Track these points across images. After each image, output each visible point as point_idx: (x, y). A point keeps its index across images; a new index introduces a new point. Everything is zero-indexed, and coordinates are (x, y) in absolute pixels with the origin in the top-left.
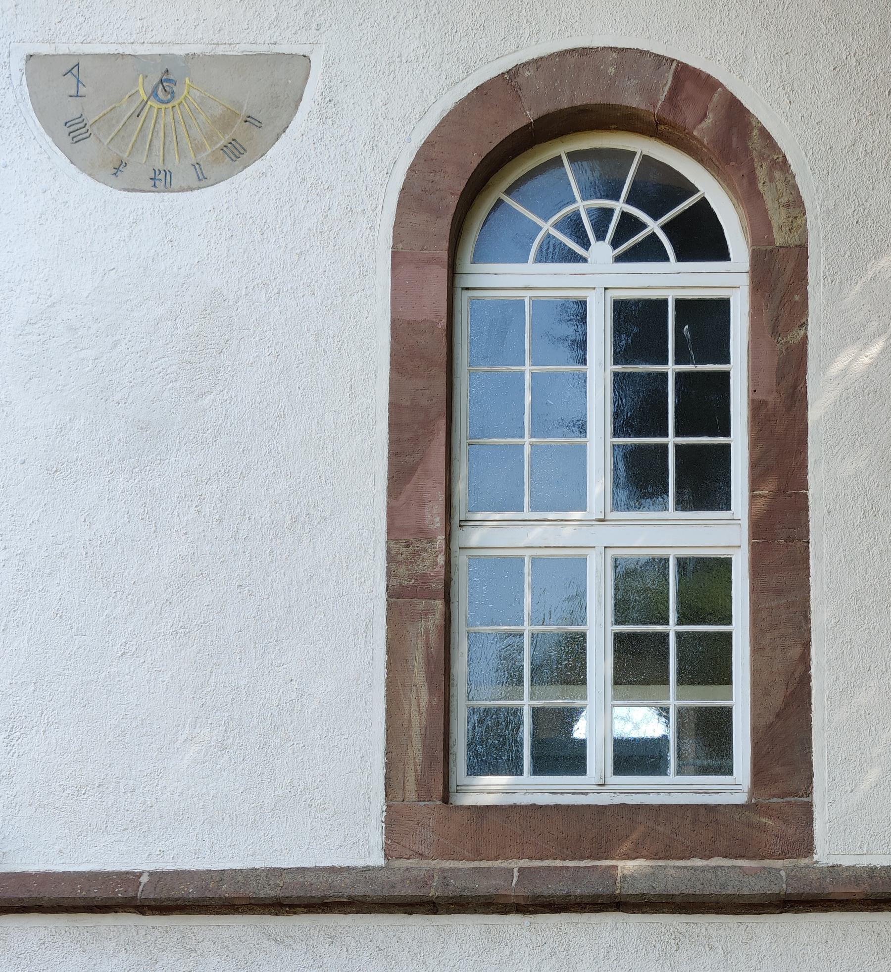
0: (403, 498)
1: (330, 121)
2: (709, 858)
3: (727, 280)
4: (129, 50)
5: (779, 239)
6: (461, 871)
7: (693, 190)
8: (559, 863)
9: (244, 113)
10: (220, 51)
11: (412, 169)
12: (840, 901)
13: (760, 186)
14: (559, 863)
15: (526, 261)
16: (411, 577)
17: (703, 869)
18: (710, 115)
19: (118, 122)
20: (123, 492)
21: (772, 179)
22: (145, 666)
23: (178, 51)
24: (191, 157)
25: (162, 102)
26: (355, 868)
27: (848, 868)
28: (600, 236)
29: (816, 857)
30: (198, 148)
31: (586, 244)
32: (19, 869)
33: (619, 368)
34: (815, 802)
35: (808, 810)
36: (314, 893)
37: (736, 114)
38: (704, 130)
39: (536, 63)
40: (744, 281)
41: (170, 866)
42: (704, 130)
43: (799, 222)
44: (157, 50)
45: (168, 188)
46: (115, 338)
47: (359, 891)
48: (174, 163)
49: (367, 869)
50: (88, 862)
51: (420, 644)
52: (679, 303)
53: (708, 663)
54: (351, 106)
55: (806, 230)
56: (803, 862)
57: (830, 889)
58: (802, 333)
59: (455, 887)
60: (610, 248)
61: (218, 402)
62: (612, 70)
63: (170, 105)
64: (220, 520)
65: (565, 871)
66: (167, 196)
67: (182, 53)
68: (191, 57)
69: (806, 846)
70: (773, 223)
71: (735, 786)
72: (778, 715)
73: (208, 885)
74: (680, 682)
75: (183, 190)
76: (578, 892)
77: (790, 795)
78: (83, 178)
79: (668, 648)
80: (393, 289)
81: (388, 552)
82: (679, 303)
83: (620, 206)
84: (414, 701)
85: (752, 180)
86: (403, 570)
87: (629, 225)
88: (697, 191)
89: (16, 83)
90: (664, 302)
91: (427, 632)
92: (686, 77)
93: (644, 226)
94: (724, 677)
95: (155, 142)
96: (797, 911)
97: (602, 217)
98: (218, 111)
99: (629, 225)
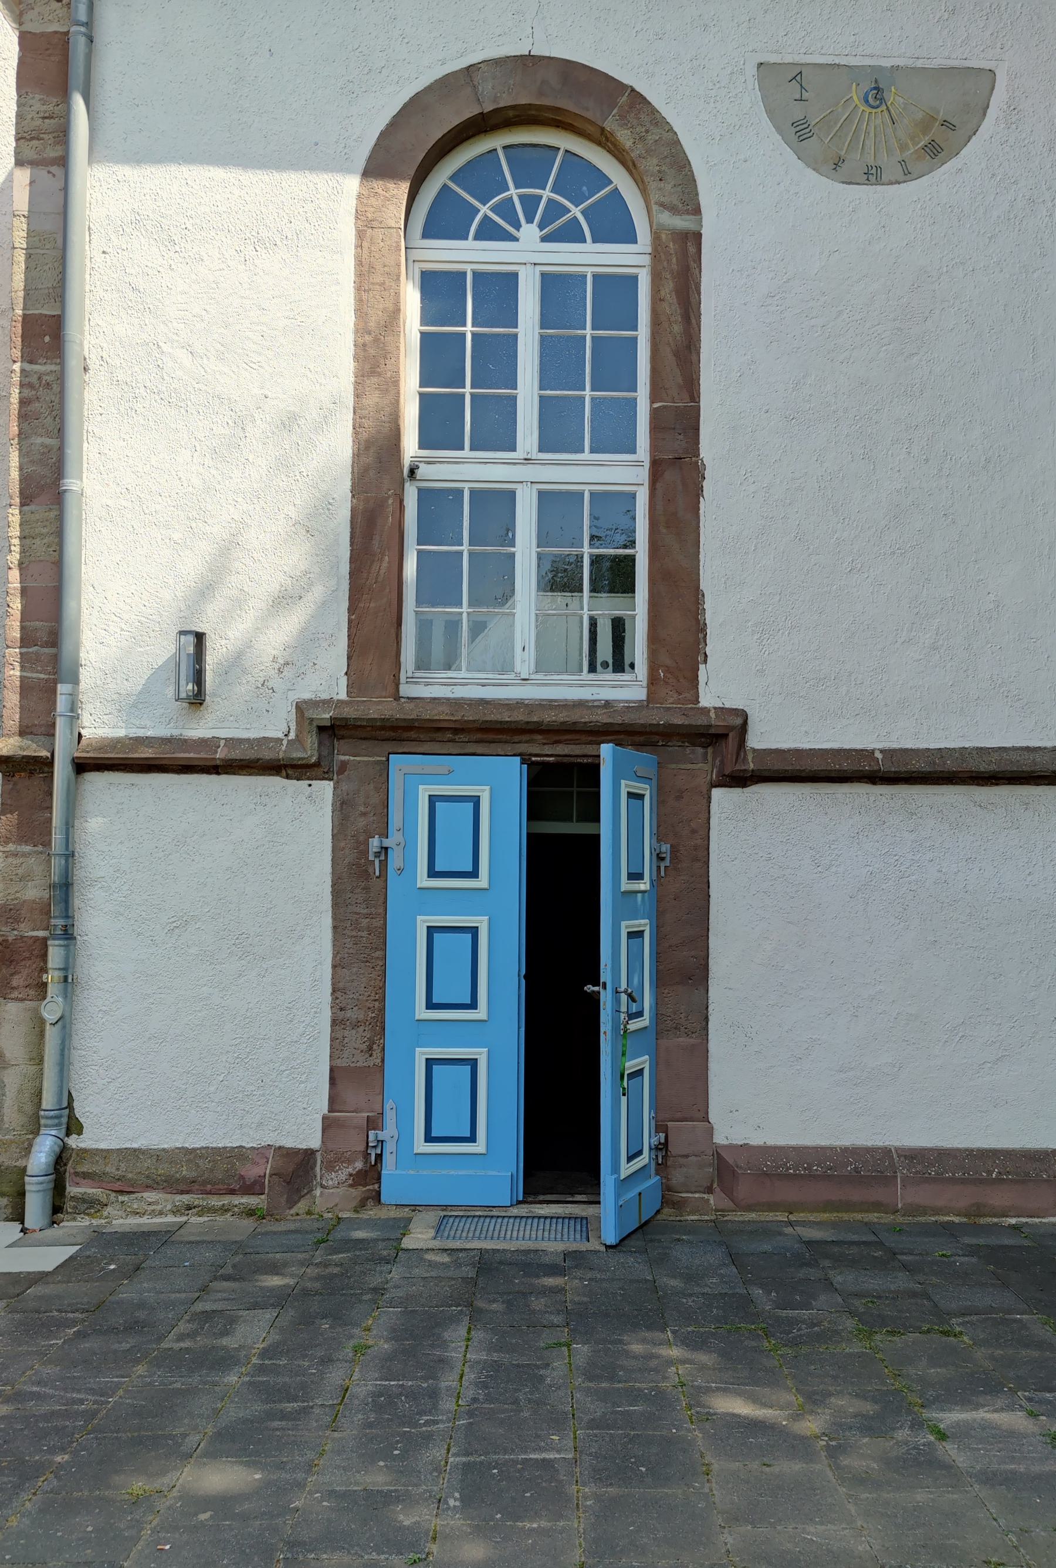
1: (1014, 126)
4: (843, 61)
9: (941, 116)
10: (919, 64)
19: (836, 123)
20: (847, 436)
22: (869, 580)
25: (873, 107)
26: (1045, 748)
30: (903, 148)
31: (518, 226)
32: (774, 746)
44: (868, 62)
45: (879, 182)
46: (839, 309)
50: (828, 741)
54: (1031, 114)
60: (538, 230)
61: (924, 362)
63: (879, 110)
64: (927, 460)
66: (879, 188)
67: (889, 65)
68: (896, 68)
73: (935, 763)
74: (594, 590)
75: (891, 183)
78: (810, 172)
89: (750, 87)
90: (464, 274)
94: (629, 588)
95: (867, 142)
98: (920, 115)
99: (554, 210)
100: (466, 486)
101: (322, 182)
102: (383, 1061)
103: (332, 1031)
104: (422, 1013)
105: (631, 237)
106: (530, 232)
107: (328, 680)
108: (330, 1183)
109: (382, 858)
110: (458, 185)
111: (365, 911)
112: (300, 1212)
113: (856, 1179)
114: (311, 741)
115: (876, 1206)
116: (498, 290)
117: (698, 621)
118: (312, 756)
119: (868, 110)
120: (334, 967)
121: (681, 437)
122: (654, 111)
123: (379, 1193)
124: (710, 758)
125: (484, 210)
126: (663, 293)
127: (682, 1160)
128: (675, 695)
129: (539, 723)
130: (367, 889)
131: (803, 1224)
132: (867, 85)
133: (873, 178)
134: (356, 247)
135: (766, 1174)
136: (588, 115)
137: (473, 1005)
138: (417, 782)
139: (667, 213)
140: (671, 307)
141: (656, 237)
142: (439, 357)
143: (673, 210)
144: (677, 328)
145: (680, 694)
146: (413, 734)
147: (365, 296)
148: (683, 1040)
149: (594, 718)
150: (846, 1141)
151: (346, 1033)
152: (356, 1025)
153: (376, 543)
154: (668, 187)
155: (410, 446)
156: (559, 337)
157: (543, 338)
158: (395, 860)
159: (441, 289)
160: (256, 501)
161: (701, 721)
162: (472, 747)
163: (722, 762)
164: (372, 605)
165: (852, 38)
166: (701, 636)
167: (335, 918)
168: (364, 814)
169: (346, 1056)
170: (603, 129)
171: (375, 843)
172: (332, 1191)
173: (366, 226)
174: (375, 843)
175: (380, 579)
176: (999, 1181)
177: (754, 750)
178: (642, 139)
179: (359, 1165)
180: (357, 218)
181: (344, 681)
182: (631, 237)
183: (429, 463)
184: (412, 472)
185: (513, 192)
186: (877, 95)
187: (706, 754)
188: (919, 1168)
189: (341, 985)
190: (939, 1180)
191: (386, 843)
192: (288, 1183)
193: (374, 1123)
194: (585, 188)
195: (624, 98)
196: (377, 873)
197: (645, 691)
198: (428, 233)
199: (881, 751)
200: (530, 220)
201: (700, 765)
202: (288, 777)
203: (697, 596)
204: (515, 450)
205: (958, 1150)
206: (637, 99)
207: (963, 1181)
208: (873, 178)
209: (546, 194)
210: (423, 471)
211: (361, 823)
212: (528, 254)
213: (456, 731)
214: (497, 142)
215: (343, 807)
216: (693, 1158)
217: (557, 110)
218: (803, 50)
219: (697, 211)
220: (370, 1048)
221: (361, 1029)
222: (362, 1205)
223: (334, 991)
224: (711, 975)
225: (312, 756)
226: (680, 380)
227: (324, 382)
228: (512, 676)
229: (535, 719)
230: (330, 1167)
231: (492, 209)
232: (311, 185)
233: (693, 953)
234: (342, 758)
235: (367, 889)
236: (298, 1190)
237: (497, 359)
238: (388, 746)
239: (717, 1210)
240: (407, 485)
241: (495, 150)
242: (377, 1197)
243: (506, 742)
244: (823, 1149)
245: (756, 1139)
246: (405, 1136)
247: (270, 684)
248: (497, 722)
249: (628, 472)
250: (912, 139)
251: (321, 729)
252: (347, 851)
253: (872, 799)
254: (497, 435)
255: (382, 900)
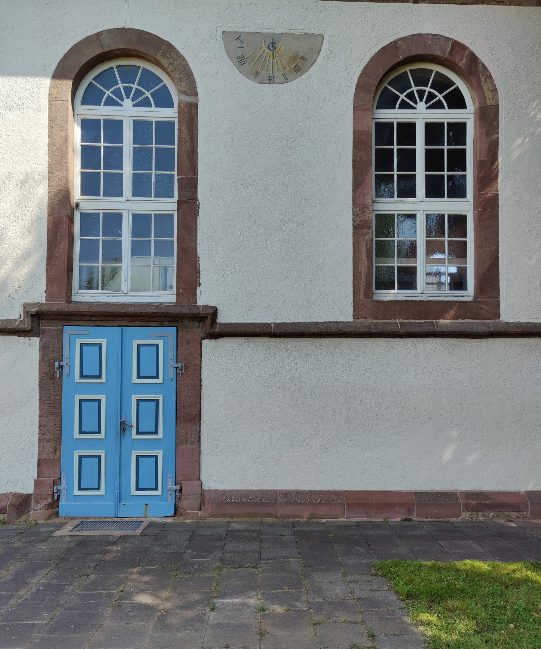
0: (358, 193)
1: (331, 59)
2: (464, 319)
3: (467, 116)
5: (489, 102)
6: (380, 322)
7: (454, 84)
8: (413, 321)
9: (300, 55)
10: (291, 32)
11: (360, 77)
12: (510, 334)
13: (482, 84)
14: (413, 321)
15: (394, 108)
16: (361, 221)
17: (463, 323)
18: (464, 58)
21: (486, 81)
23: (277, 32)
24: (282, 71)
25: (271, 51)
27: (512, 323)
28: (421, 100)
29: (501, 319)
30: (284, 68)
31: (416, 103)
32: (229, 322)
33: (428, 147)
34: (501, 300)
35: (498, 303)
36: (333, 331)
37: (473, 59)
38: (462, 63)
39: (403, 39)
40: (472, 116)
41: (280, 321)
42: (462, 63)
43: (496, 96)
44: (269, 31)
45: (274, 83)
47: (348, 330)
48: (276, 73)
49: (347, 322)
51: (364, 244)
52: (449, 124)
53: (459, 251)
55: (498, 100)
56: (496, 321)
57: (509, 330)
58: (497, 136)
59: (380, 329)
62: (430, 42)
65: (420, 324)
69: (498, 316)
70: (487, 97)
71: (469, 293)
72: (488, 270)
73: (295, 329)
75: (279, 83)
76: (423, 330)
77: (492, 298)
78: (244, 78)
79: (445, 246)
80: (354, 120)
81: (353, 212)
82: (449, 124)
83: (428, 89)
84: (362, 264)
85: (479, 82)
86: (358, 219)
87: (431, 96)
88: (455, 84)
91: (367, 240)
92: (457, 46)
93: (436, 96)
95: (269, 66)
96: (495, 338)
97: (421, 93)
98: (291, 54)
99: (138, 93)
100: (101, 212)
101: (33, 81)
102: (61, 456)
103: (39, 444)
104: (77, 436)
105: (170, 105)
106: (128, 103)
107: (38, 295)
108: (37, 508)
109: (60, 370)
110: (97, 82)
111: (53, 393)
112: (22, 521)
113: (261, 504)
114: (28, 321)
115: (269, 515)
116: (114, 128)
117: (196, 269)
118: (28, 327)
119: (270, 52)
120: (40, 416)
121: (190, 191)
122: (177, 52)
123: (58, 512)
124: (201, 327)
125: (108, 93)
126: (182, 129)
127: (187, 497)
128: (187, 301)
129: (126, 313)
130: (54, 383)
131: (236, 522)
132: (269, 41)
133: (272, 81)
134: (49, 109)
135: (222, 502)
136: (149, 53)
137: (99, 432)
138: (76, 338)
139: (183, 95)
140: (185, 135)
141: (179, 105)
142: (89, 156)
143: (186, 94)
144: (188, 145)
145: (189, 300)
146: (73, 318)
147: (53, 130)
148: (189, 446)
149: (149, 310)
150: (258, 488)
151: (45, 444)
152: (49, 441)
153: (58, 236)
154: (184, 84)
155: (76, 195)
156: (141, 148)
157: (134, 149)
158: (65, 371)
159: (89, 127)
160: (5, 218)
161: (196, 311)
162: (99, 323)
163: (206, 329)
164: (57, 262)
165: (263, 21)
166: (198, 275)
167: (40, 395)
168: (53, 352)
169: (45, 454)
170: (156, 59)
171: (57, 364)
172: (37, 512)
173: (53, 99)
174: (57, 364)
175: (60, 251)
176: (320, 504)
177: (220, 323)
178: (172, 63)
179: (50, 500)
180: (49, 96)
181: (44, 295)
182: (172, 106)
183: (85, 202)
184: (77, 205)
185: (121, 85)
186: (273, 46)
187: (199, 325)
188: (287, 498)
189: (43, 424)
190: (295, 503)
191: (62, 364)
192: (17, 509)
193: (56, 482)
194: (151, 84)
195: (164, 46)
196: (58, 377)
197: (176, 298)
198: (84, 102)
199: (274, 324)
200: (128, 97)
201: (197, 330)
202: (19, 336)
203: (196, 259)
204: (122, 196)
205: (306, 491)
206: (170, 47)
207: (304, 504)
208: (272, 81)
209: (135, 86)
210: (82, 205)
211: (51, 355)
212: (127, 112)
213: (91, 316)
214: (113, 64)
215: (44, 349)
216: (192, 496)
217: (136, 51)
218: (241, 26)
219: (196, 94)
220: (55, 451)
221: (51, 443)
222: (50, 517)
223: (40, 427)
224: (202, 419)
225: (28, 327)
226: (189, 167)
227: (35, 166)
228: (120, 292)
229: (124, 311)
230: (37, 501)
231: (112, 93)
232: (29, 83)
233: (194, 409)
234: (43, 328)
235: (54, 383)
236: (22, 512)
237: (114, 157)
238: (63, 323)
239: (201, 518)
240: (75, 211)
241: (113, 68)
242: (57, 513)
243: (113, 321)
244: (248, 491)
245: (220, 488)
246: (69, 488)
247: (12, 296)
248: (108, 312)
249: (168, 206)
250: (288, 64)
251: (32, 316)
252: (45, 367)
253: (271, 344)
254: (114, 188)
255: (60, 388)
